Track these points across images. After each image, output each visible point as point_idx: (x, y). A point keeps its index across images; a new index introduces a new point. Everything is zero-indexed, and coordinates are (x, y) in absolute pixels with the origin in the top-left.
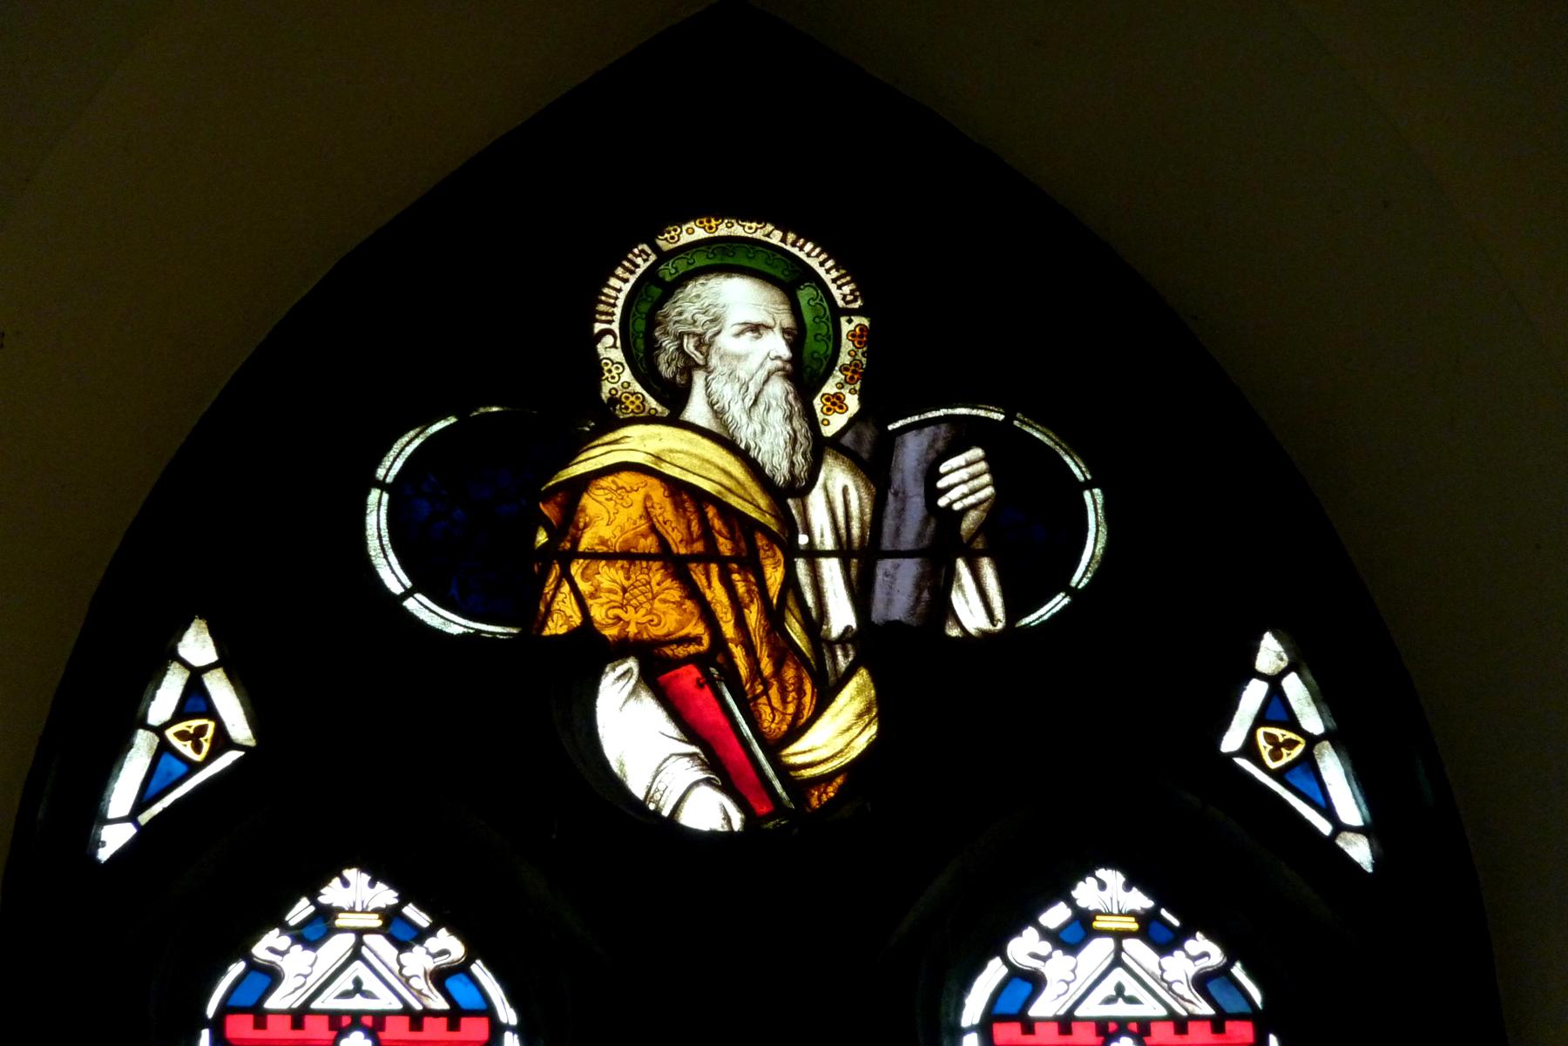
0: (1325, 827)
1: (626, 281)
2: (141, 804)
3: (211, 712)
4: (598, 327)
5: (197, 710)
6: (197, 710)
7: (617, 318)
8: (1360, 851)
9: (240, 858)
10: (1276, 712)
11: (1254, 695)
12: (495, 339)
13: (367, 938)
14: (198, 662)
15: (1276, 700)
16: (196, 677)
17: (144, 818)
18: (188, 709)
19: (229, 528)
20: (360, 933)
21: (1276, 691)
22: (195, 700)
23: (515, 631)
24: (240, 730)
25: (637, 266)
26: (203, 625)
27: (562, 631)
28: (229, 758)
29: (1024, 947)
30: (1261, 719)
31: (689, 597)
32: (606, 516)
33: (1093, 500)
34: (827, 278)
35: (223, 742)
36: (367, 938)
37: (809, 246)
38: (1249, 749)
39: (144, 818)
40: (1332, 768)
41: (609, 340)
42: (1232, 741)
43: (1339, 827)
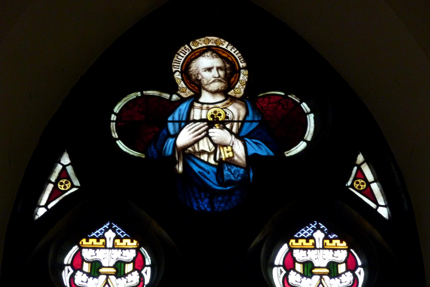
0: (373, 205)
1: (183, 57)
5: (64, 177)
6: (64, 177)
7: (181, 63)
8: (384, 212)
9: (78, 221)
10: (359, 175)
12: (145, 62)
14: (65, 164)
15: (359, 171)
16: (64, 167)
20: (108, 275)
21: (360, 170)
25: (186, 53)
26: (68, 155)
28: (74, 190)
29: (300, 233)
30: (355, 178)
31: (214, 53)
33: (311, 118)
34: (237, 56)
35: (73, 186)
36: (110, 277)
38: (352, 186)
39: (50, 206)
41: (178, 73)
43: (378, 205)
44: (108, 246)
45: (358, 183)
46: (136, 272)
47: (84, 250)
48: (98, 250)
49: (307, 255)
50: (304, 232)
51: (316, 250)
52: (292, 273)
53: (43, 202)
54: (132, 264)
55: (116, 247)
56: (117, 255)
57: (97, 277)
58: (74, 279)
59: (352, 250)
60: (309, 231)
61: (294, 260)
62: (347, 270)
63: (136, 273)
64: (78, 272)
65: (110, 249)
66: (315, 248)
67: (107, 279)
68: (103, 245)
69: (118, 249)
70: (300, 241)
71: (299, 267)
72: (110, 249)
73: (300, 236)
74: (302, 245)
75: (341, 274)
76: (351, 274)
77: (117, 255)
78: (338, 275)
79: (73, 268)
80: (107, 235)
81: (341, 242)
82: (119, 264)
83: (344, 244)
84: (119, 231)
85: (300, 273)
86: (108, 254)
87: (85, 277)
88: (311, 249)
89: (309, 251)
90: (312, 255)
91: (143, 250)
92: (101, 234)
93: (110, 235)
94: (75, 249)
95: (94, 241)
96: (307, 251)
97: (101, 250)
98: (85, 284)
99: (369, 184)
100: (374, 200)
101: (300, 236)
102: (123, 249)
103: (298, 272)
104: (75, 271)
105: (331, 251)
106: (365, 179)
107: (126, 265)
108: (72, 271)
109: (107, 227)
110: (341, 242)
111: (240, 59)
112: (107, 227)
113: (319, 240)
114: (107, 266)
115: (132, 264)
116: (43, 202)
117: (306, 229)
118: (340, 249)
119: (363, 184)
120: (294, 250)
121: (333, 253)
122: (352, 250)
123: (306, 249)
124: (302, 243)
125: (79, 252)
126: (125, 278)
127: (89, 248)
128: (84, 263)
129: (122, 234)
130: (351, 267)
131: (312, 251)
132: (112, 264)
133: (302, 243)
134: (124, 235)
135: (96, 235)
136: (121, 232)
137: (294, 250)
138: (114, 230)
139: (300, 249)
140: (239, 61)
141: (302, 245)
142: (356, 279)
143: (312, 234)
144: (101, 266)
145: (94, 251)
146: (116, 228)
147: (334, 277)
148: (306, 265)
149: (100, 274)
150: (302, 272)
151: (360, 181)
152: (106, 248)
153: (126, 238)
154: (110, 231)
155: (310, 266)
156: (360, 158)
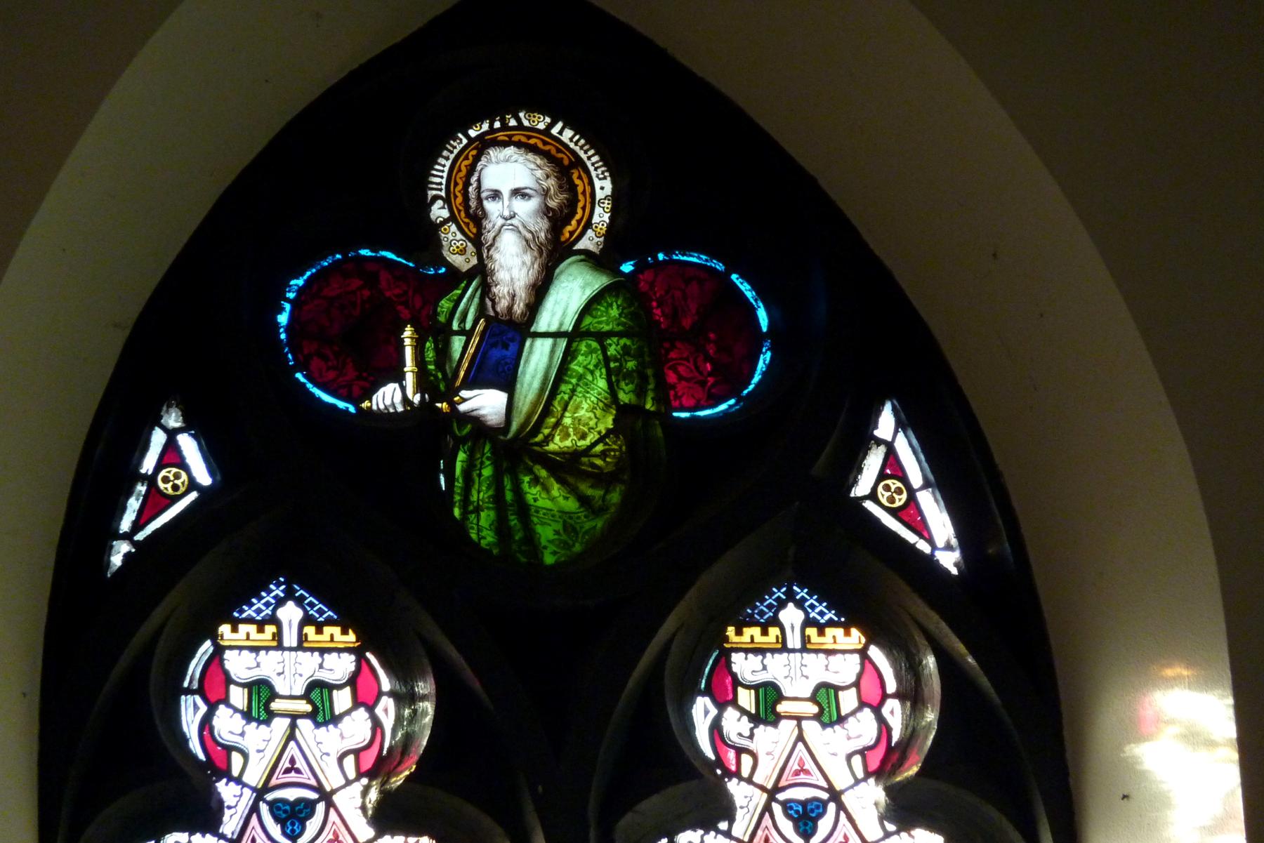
2: (138, 526)
3: (182, 464)
4: (431, 193)
6: (180, 462)
11: (874, 461)
12: (338, 192)
13: (300, 722)
17: (140, 537)
18: (166, 460)
19: (185, 343)
20: (294, 717)
22: (171, 455)
23: (745, 392)
24: (204, 479)
27: (956, 555)
30: (882, 476)
32: (313, 796)
36: (300, 722)
37: (591, 152)
38: (873, 496)
39: (140, 537)
40: (929, 502)
41: (440, 203)
42: (862, 488)
44: (286, 644)
45: (887, 488)
46: (362, 710)
47: (228, 655)
48: (263, 653)
49: (765, 668)
50: (258, 607)
51: (785, 655)
52: (222, 710)
53: (125, 525)
54: (348, 689)
55: (306, 645)
56: (307, 666)
57: (267, 722)
58: (211, 729)
59: (368, 655)
60: (267, 604)
61: (228, 680)
62: (357, 703)
63: (867, 714)
64: (222, 707)
65: (291, 649)
66: (784, 649)
67: (293, 726)
68: (273, 639)
69: (312, 650)
70: (243, 628)
71: (238, 696)
72: (291, 649)
73: (244, 615)
74: (332, 640)
75: (342, 716)
76: (367, 715)
77: (307, 666)
78: (335, 720)
79: (206, 699)
80: (282, 613)
81: (345, 632)
82: (823, 691)
83: (351, 637)
84: (812, 607)
85: (242, 712)
86: (287, 662)
87: (238, 720)
88: (773, 651)
89: (769, 655)
90: (269, 666)
91: (875, 653)
92: (269, 611)
93: (290, 614)
94: (207, 647)
95: (756, 631)
96: (764, 657)
97: (271, 652)
98: (239, 739)
99: (912, 493)
100: (921, 528)
101: (244, 615)
102: (323, 651)
103: (236, 710)
104: (212, 708)
105: (316, 654)
106: (903, 478)
107: (335, 692)
108: (714, 711)
109: (282, 595)
110: (345, 632)
111: (596, 169)
112: (282, 595)
113: (793, 627)
114: (287, 693)
115: (348, 689)
116: (125, 525)
117: (261, 598)
118: (844, 652)
119: (899, 491)
120: (733, 655)
121: (320, 660)
122: (368, 655)
123: (255, 649)
124: (752, 637)
125: (216, 661)
126: (336, 726)
127: (240, 648)
128: (232, 687)
129: (321, 612)
130: (365, 700)
131: (776, 655)
132: (299, 690)
133: (752, 637)
134: (826, 618)
135: (254, 615)
136: (318, 608)
137: (733, 655)
138: (300, 602)
139: (747, 651)
140: (593, 174)
141: (332, 640)
142: (377, 725)
143: (274, 611)
144: (780, 697)
145: (254, 655)
146: (803, 600)
147: (326, 723)
148: (255, 689)
149: (271, 715)
150: (753, 711)
151: (894, 484)
152: (280, 647)
153: (329, 622)
154: (791, 605)
155: (265, 694)
156: (886, 424)
